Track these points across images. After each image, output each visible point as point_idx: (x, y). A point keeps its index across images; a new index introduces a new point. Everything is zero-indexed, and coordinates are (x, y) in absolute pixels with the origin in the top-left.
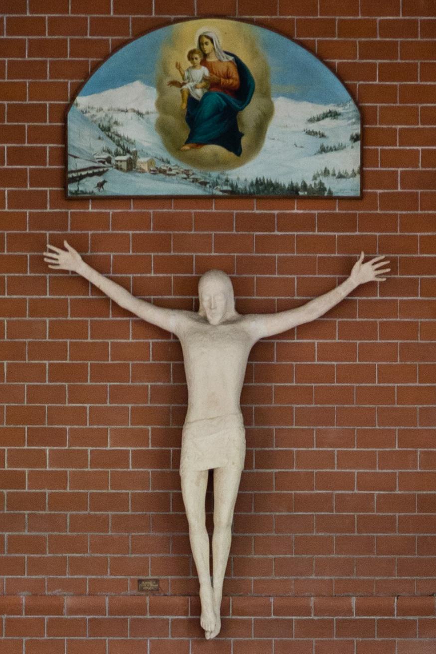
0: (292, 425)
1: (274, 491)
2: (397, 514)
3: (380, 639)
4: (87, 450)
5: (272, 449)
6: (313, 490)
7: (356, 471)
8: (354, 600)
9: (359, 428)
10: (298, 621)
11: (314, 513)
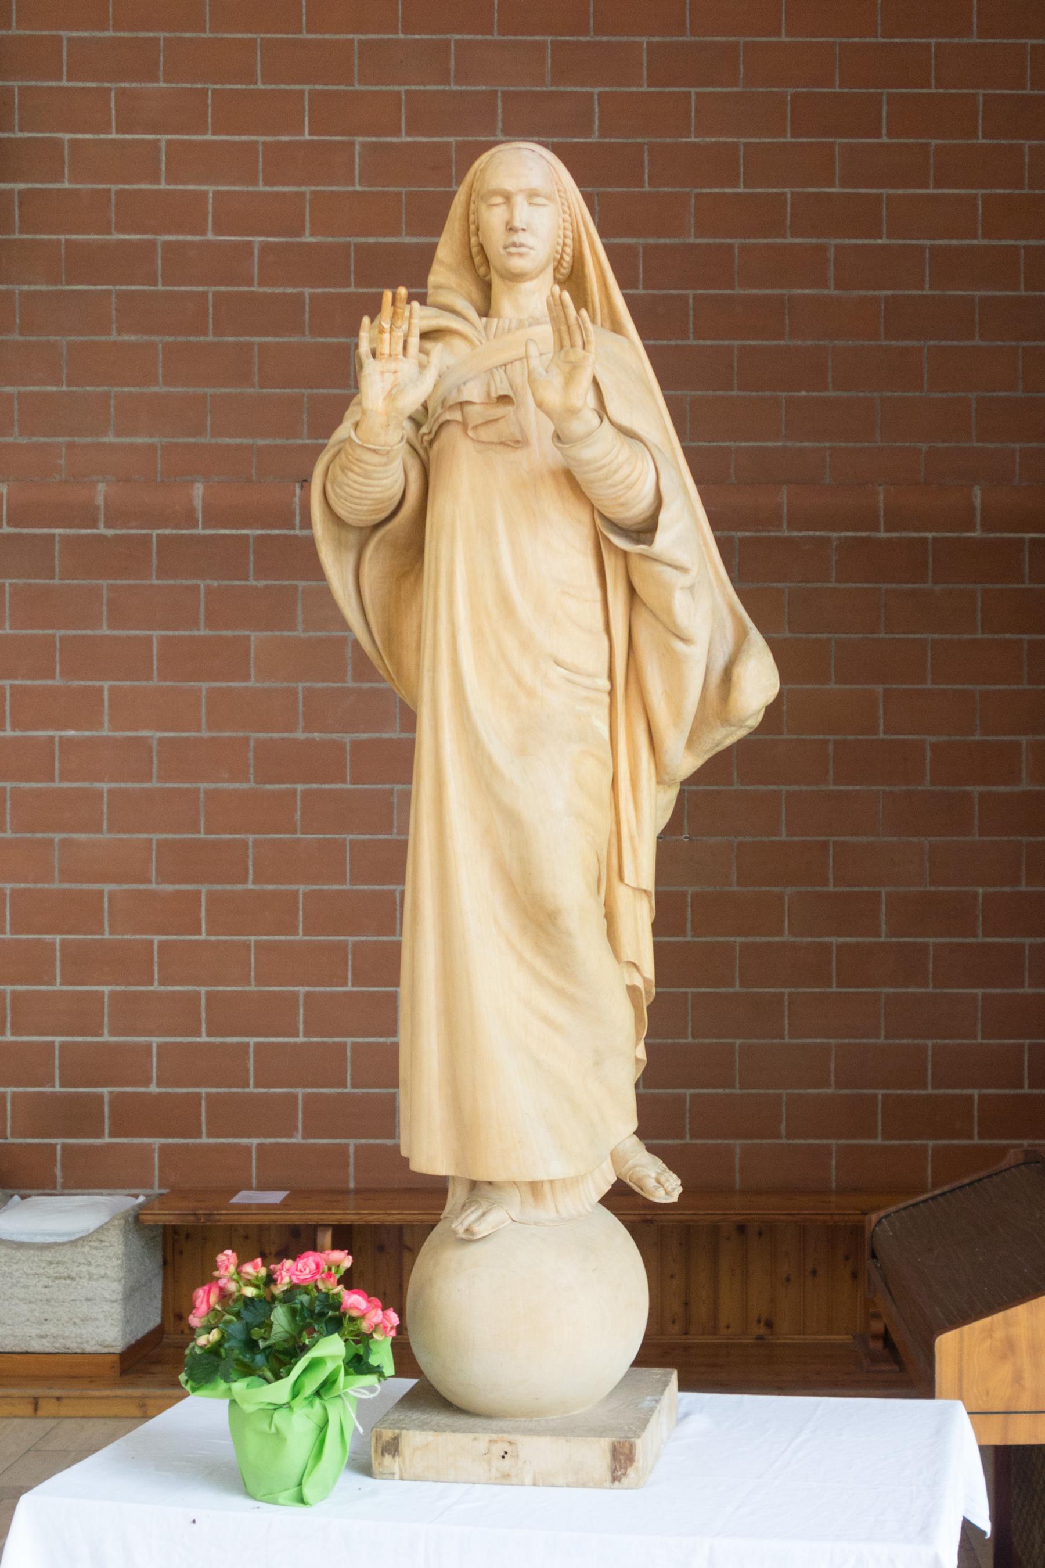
0: (59, 78)
1: (17, 236)
2: (307, 291)
3: (261, 583)
4: (304, 935)
5: (12, 135)
6: (110, 233)
7: (210, 189)
8: (198, 490)
9: (218, 86)
10: (65, 539)
11: (110, 287)
